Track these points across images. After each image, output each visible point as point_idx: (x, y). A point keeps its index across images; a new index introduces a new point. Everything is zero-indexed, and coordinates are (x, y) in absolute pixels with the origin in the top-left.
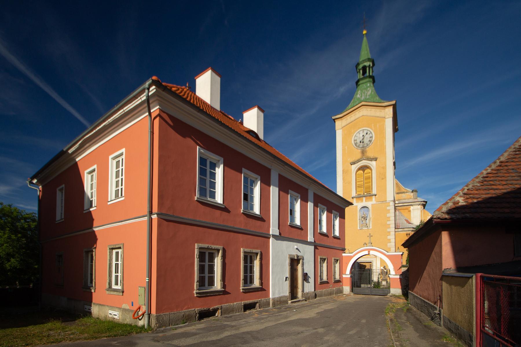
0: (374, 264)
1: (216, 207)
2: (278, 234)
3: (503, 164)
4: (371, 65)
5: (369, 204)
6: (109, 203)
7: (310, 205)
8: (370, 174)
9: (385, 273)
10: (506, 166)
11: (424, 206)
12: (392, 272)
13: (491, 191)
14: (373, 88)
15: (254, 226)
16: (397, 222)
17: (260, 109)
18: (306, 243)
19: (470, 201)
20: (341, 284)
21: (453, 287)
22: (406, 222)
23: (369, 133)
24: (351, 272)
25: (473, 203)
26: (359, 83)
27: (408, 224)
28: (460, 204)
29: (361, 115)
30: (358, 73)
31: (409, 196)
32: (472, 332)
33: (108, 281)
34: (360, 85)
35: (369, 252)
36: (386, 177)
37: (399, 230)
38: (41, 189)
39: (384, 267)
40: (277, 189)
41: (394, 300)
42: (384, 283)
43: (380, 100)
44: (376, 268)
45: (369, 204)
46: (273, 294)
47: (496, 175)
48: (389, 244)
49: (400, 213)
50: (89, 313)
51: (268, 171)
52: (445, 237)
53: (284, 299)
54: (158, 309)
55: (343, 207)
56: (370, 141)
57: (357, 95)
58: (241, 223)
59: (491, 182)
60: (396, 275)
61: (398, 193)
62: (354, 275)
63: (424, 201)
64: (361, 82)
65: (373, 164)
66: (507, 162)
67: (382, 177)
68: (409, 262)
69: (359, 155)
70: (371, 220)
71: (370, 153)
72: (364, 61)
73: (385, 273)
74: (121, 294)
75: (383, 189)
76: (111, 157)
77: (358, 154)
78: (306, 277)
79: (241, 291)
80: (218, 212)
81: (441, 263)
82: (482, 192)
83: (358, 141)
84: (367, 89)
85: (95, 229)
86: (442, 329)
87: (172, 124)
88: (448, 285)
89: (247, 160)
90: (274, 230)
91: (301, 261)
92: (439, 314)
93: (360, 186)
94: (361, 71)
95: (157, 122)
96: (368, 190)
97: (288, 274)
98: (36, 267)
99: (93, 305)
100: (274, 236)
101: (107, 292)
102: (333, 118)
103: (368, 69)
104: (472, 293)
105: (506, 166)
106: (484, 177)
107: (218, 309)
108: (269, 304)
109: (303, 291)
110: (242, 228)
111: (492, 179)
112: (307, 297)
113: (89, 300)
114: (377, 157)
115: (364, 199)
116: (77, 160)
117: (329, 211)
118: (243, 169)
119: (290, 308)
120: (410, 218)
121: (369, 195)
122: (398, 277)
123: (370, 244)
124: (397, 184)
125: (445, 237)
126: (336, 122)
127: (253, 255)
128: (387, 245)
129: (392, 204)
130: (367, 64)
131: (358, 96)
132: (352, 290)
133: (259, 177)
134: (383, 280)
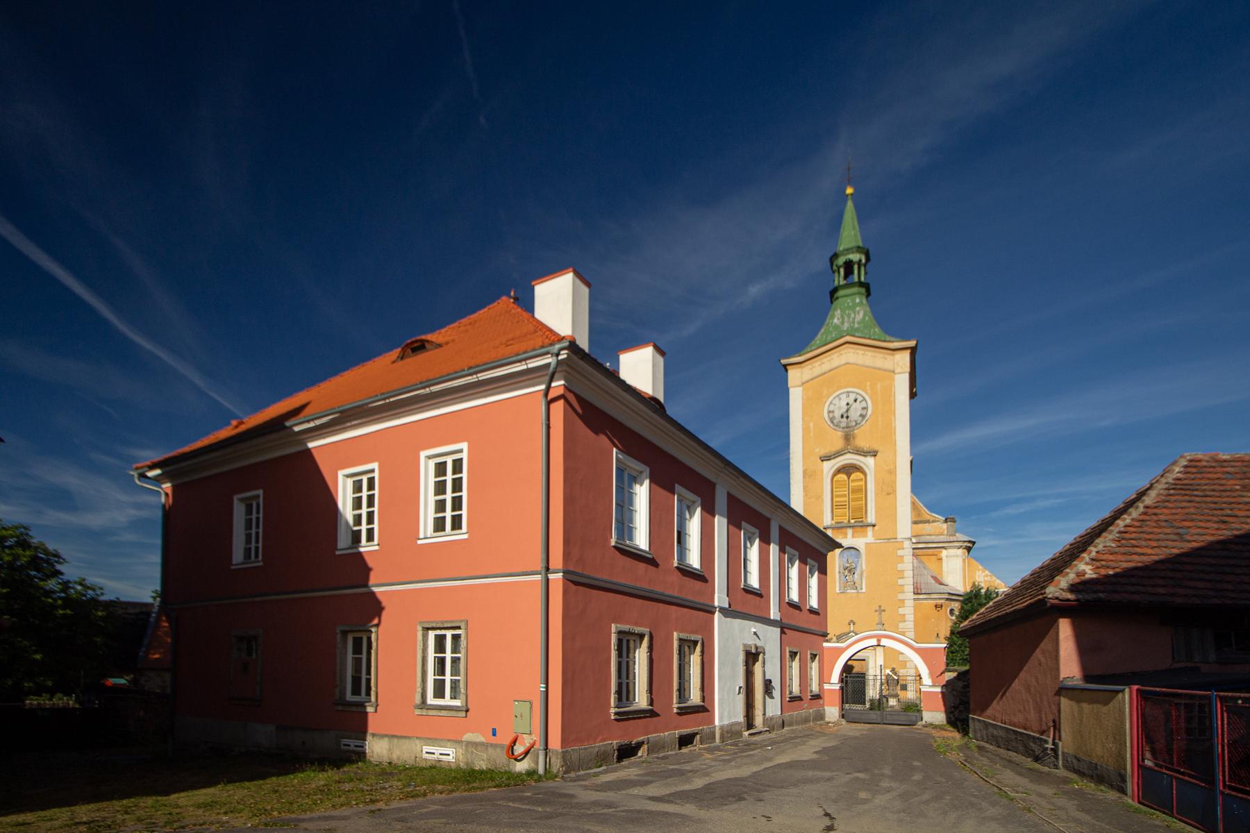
0: (871, 664)
1: (637, 556)
2: (727, 606)
3: (1150, 511)
6: (419, 542)
7: (774, 549)
9: (894, 682)
11: (969, 549)
15: (690, 590)
18: (767, 621)
19: (1103, 572)
21: (1085, 706)
23: (860, 399)
24: (841, 680)
25: (1107, 576)
28: (1087, 576)
29: (843, 362)
31: (938, 528)
32: (1125, 769)
33: (419, 690)
34: (840, 300)
35: (879, 641)
36: (895, 491)
38: (170, 492)
39: (893, 670)
43: (883, 336)
44: (875, 668)
45: (860, 542)
46: (721, 718)
49: (921, 562)
50: (361, 755)
51: (711, 486)
52: (1065, 628)
53: (738, 728)
54: (565, 741)
55: (823, 551)
56: (863, 416)
57: (833, 317)
58: (673, 586)
60: (934, 686)
61: (915, 523)
64: (841, 293)
67: (888, 490)
71: (862, 442)
72: (849, 251)
73: (894, 682)
74: (463, 714)
75: (889, 513)
76: (423, 454)
78: (768, 685)
80: (642, 566)
81: (1058, 669)
82: (1120, 557)
83: (837, 414)
84: (852, 311)
85: (375, 589)
86: (1062, 772)
87: (580, 411)
88: (1073, 703)
89: (683, 469)
90: (720, 598)
91: (761, 656)
92: (1055, 750)
93: (841, 506)
94: (842, 271)
95: (558, 408)
96: (857, 515)
97: (741, 682)
98: (38, 657)
99: (369, 738)
100: (722, 610)
101: (418, 712)
102: (784, 361)
103: (856, 267)
104: (1124, 712)
106: (1120, 532)
110: (676, 595)
111: (1133, 536)
112: (771, 725)
113: (361, 730)
115: (850, 531)
117: (803, 561)
119: (749, 746)
120: (941, 574)
121: (861, 525)
122: (939, 690)
124: (913, 503)
125: (1065, 628)
127: (632, 638)
130: (855, 257)
131: (836, 321)
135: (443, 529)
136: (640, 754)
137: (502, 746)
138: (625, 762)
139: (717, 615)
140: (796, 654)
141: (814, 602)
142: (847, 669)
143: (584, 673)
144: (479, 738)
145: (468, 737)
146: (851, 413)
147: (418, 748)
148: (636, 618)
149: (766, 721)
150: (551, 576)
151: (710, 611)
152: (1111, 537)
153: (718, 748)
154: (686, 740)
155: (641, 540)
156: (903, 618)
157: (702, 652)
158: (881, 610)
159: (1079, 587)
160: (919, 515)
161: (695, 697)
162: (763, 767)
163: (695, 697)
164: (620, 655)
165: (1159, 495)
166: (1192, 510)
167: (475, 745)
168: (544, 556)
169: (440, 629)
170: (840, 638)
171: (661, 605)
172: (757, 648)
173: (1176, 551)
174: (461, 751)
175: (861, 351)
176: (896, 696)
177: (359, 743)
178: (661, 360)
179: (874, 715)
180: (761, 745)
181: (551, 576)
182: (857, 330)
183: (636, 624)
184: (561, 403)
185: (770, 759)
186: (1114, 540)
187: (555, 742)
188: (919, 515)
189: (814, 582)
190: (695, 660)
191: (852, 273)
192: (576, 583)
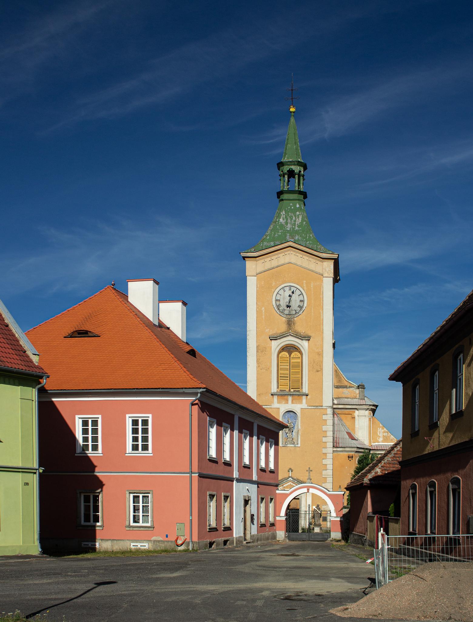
8: (300, 360)
9: (318, 515)
11: (374, 411)
16: (335, 436)
17: (184, 304)
18: (252, 482)
19: (384, 472)
20: (275, 528)
22: (348, 437)
24: (286, 514)
25: (386, 474)
27: (350, 440)
29: (287, 261)
31: (352, 394)
35: (308, 490)
36: (322, 369)
37: (339, 449)
39: (318, 506)
41: (335, 543)
42: (317, 530)
44: (306, 506)
45: (297, 408)
48: (324, 472)
49: (340, 420)
53: (241, 539)
54: (199, 538)
56: (300, 307)
60: (337, 517)
61: (337, 387)
63: (373, 405)
64: (285, 196)
65: (304, 345)
67: (317, 368)
69: (283, 328)
70: (300, 433)
71: (300, 328)
73: (318, 515)
77: (281, 325)
82: (391, 466)
83: (283, 304)
90: (236, 475)
94: (286, 176)
97: (243, 517)
106: (395, 454)
114: (309, 335)
115: (290, 398)
120: (354, 429)
121: (297, 393)
122: (339, 519)
124: (336, 371)
128: (321, 474)
129: (330, 411)
131: (281, 220)
135: (137, 449)
136: (213, 546)
137: (172, 542)
139: (235, 481)
141: (272, 466)
144: (160, 538)
145: (154, 538)
147: (128, 544)
149: (252, 536)
151: (232, 480)
156: (325, 467)
158: (310, 470)
159: (376, 478)
160: (340, 380)
167: (159, 541)
169: (137, 493)
174: (150, 544)
175: (300, 254)
176: (319, 525)
177: (93, 543)
179: (304, 536)
182: (297, 232)
187: (195, 538)
188: (340, 380)
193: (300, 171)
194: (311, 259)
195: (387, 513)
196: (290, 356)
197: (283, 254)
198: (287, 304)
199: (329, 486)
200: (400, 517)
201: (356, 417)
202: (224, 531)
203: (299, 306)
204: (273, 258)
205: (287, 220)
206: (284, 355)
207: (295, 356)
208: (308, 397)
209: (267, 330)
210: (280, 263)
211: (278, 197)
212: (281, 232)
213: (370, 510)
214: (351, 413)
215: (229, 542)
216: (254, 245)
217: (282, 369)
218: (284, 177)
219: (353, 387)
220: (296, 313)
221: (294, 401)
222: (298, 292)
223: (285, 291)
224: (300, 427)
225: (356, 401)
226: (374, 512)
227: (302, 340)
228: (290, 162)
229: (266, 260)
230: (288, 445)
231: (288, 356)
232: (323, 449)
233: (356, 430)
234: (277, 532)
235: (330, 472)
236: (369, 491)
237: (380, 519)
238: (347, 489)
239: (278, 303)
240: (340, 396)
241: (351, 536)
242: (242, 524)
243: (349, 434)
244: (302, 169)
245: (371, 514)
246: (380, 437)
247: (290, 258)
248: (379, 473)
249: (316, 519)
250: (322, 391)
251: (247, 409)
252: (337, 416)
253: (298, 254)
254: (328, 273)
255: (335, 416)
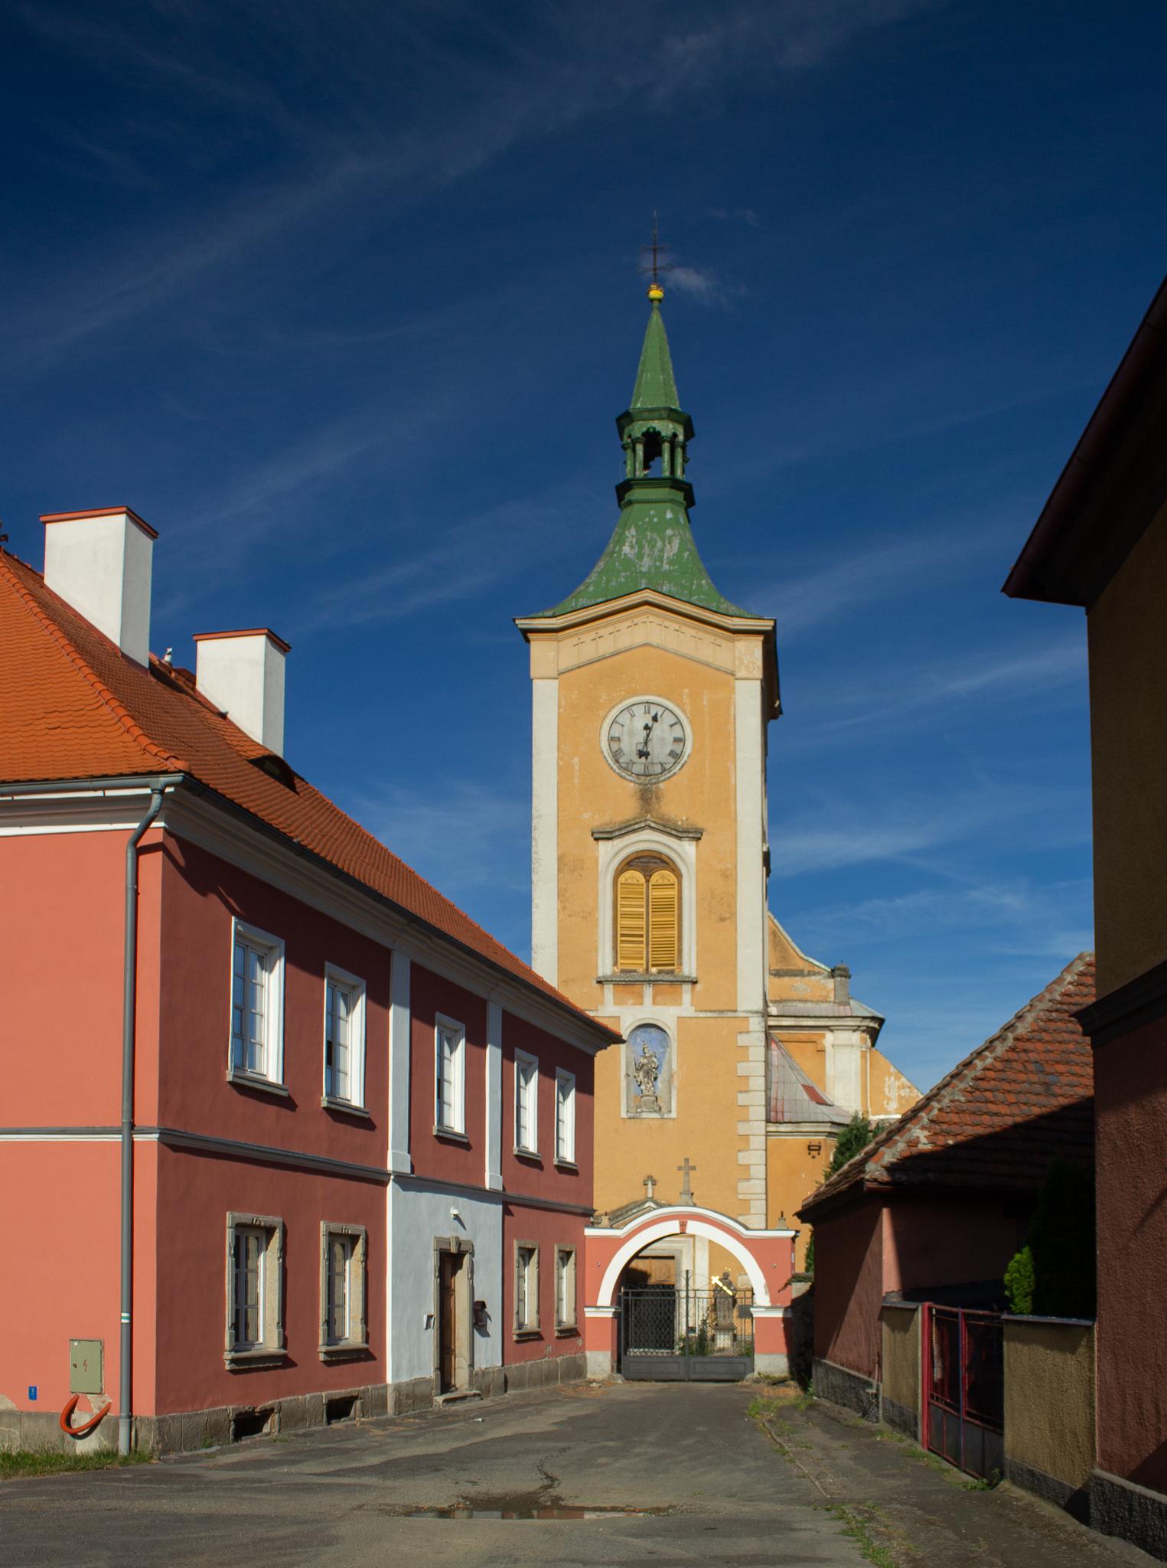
2: (408, 1170)
3: (1021, 1045)
4: (681, 438)
5: (667, 1015)
7: (492, 1055)
8: (674, 892)
9: (729, 1301)
10: (1025, 1051)
11: (874, 1035)
12: (762, 1298)
13: (986, 1119)
14: (689, 535)
15: (346, 1145)
16: (773, 1095)
20: (580, 1342)
22: (806, 1097)
24: (617, 1299)
26: (628, 496)
27: (813, 1104)
28: (920, 1147)
30: (624, 448)
35: (683, 1225)
36: (734, 914)
37: (783, 1128)
39: (725, 1278)
40: (406, 1013)
41: (768, 1391)
42: (723, 1341)
44: (697, 1280)
45: (667, 1015)
46: (396, 1372)
47: (1001, 1075)
48: (743, 1186)
49: (786, 1055)
53: (423, 1389)
54: (161, 1403)
55: (588, 1050)
56: (675, 756)
57: (621, 542)
58: (316, 1140)
59: (988, 1094)
60: (773, 1308)
61: (778, 974)
62: (627, 1310)
63: (873, 1018)
64: (636, 494)
65: (686, 852)
66: (1029, 1040)
67: (721, 911)
68: (815, 1260)
70: (676, 1083)
71: (674, 805)
73: (729, 1301)
75: (722, 957)
77: (623, 802)
78: (479, 1311)
79: (322, 1357)
80: (272, 1110)
82: (967, 1118)
83: (629, 747)
84: (654, 537)
87: (182, 862)
90: (396, 1158)
93: (631, 936)
94: (640, 448)
97: (432, 1308)
102: (522, 623)
103: (666, 446)
105: (1025, 1051)
106: (977, 1079)
107: (271, 1411)
108: (385, 1405)
109: (472, 1365)
110: (324, 1156)
114: (700, 825)
115: (648, 991)
116: (487, 1187)
117: (547, 1072)
118: (327, 963)
119: (444, 1418)
120: (822, 1079)
121: (668, 979)
122: (779, 1314)
123: (686, 1197)
124: (774, 934)
126: (532, 644)
128: (735, 1189)
129: (756, 1024)
130: (666, 428)
131: (626, 549)
132: (619, 1365)
133: (364, 984)
134: (718, 1328)
136: (266, 1429)
137: (50, 1417)
138: (246, 1441)
139: (390, 1187)
140: (531, 1252)
141: (567, 1152)
142: (631, 1278)
143: (190, 1295)
146: (654, 748)
148: (262, 1197)
150: (137, 1138)
151: (379, 1180)
152: (962, 1086)
153: (392, 1422)
154: (338, 1409)
155: (270, 1066)
157: (366, 1254)
158: (688, 1167)
161: (352, 1333)
162: (467, 1442)
163: (352, 1333)
164: (237, 1265)
165: (1037, 1019)
166: (1071, 1047)
168: (127, 1105)
170: (618, 1217)
171: (300, 1175)
172: (459, 1244)
173: (1036, 1111)
175: (673, 623)
176: (729, 1328)
178: (280, 659)
180: (467, 1417)
181: (137, 1138)
182: (667, 576)
183: (262, 1211)
184: (158, 857)
185: (480, 1434)
186: (965, 1091)
187: (146, 1405)
189: (567, 1110)
190: (352, 1269)
191: (660, 454)
192: (176, 1148)
193: (675, 435)
194: (701, 635)
195: (997, 1298)
196: (648, 881)
197: (629, 623)
198: (640, 747)
199: (756, 1219)
200: (1091, 1315)
201: (829, 1049)
202: (517, 1342)
203: (672, 754)
204: (601, 632)
205: (641, 547)
206: (632, 878)
207: (660, 882)
208: (698, 987)
209: (586, 816)
210: (620, 646)
211: (620, 498)
212: (626, 577)
213: (890, 1280)
214: (814, 1038)
215: (358, 1403)
216: (552, 598)
217: (625, 915)
218: (634, 451)
219: (819, 973)
220: (664, 770)
221: (659, 998)
222: (667, 719)
223: (633, 716)
224: (674, 1067)
225: (825, 1009)
226: (911, 1290)
227: (680, 838)
228: (651, 410)
229: (583, 638)
230: (644, 1115)
231: (642, 880)
232: (740, 1125)
233: (829, 1082)
234: (588, 1354)
235: (759, 1186)
236: (885, 1214)
237: (944, 1324)
238: (803, 1215)
239: (615, 746)
240: (784, 997)
241: (817, 1373)
242: (431, 1337)
243: (810, 1091)
244: (680, 432)
245: (896, 1301)
246: (889, 1099)
247: (648, 631)
248: (925, 1145)
249: (720, 1314)
250: (734, 973)
251: (443, 936)
252: (779, 1047)
253: (667, 623)
254: (747, 668)
255: (774, 1046)
